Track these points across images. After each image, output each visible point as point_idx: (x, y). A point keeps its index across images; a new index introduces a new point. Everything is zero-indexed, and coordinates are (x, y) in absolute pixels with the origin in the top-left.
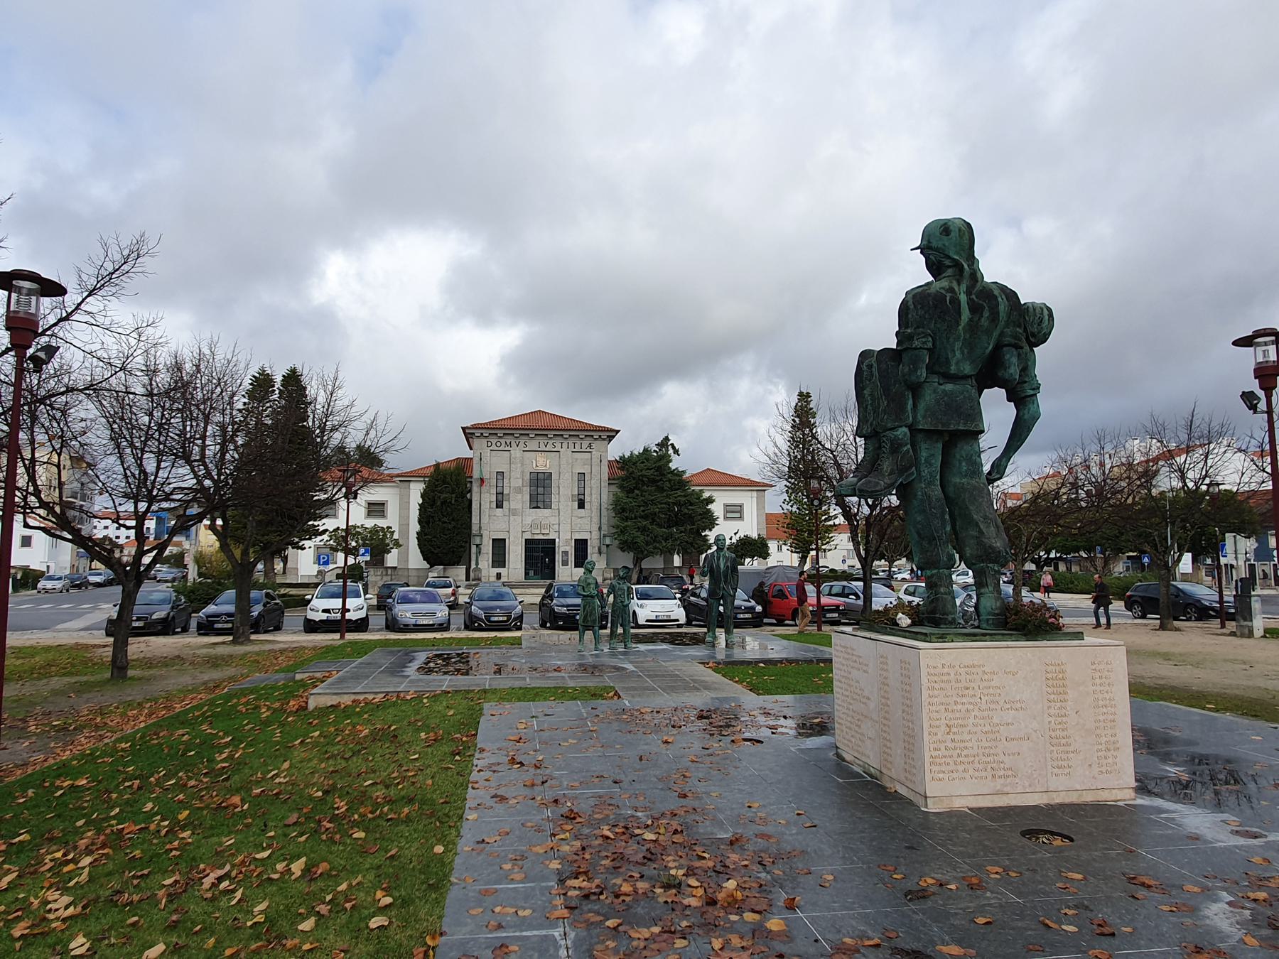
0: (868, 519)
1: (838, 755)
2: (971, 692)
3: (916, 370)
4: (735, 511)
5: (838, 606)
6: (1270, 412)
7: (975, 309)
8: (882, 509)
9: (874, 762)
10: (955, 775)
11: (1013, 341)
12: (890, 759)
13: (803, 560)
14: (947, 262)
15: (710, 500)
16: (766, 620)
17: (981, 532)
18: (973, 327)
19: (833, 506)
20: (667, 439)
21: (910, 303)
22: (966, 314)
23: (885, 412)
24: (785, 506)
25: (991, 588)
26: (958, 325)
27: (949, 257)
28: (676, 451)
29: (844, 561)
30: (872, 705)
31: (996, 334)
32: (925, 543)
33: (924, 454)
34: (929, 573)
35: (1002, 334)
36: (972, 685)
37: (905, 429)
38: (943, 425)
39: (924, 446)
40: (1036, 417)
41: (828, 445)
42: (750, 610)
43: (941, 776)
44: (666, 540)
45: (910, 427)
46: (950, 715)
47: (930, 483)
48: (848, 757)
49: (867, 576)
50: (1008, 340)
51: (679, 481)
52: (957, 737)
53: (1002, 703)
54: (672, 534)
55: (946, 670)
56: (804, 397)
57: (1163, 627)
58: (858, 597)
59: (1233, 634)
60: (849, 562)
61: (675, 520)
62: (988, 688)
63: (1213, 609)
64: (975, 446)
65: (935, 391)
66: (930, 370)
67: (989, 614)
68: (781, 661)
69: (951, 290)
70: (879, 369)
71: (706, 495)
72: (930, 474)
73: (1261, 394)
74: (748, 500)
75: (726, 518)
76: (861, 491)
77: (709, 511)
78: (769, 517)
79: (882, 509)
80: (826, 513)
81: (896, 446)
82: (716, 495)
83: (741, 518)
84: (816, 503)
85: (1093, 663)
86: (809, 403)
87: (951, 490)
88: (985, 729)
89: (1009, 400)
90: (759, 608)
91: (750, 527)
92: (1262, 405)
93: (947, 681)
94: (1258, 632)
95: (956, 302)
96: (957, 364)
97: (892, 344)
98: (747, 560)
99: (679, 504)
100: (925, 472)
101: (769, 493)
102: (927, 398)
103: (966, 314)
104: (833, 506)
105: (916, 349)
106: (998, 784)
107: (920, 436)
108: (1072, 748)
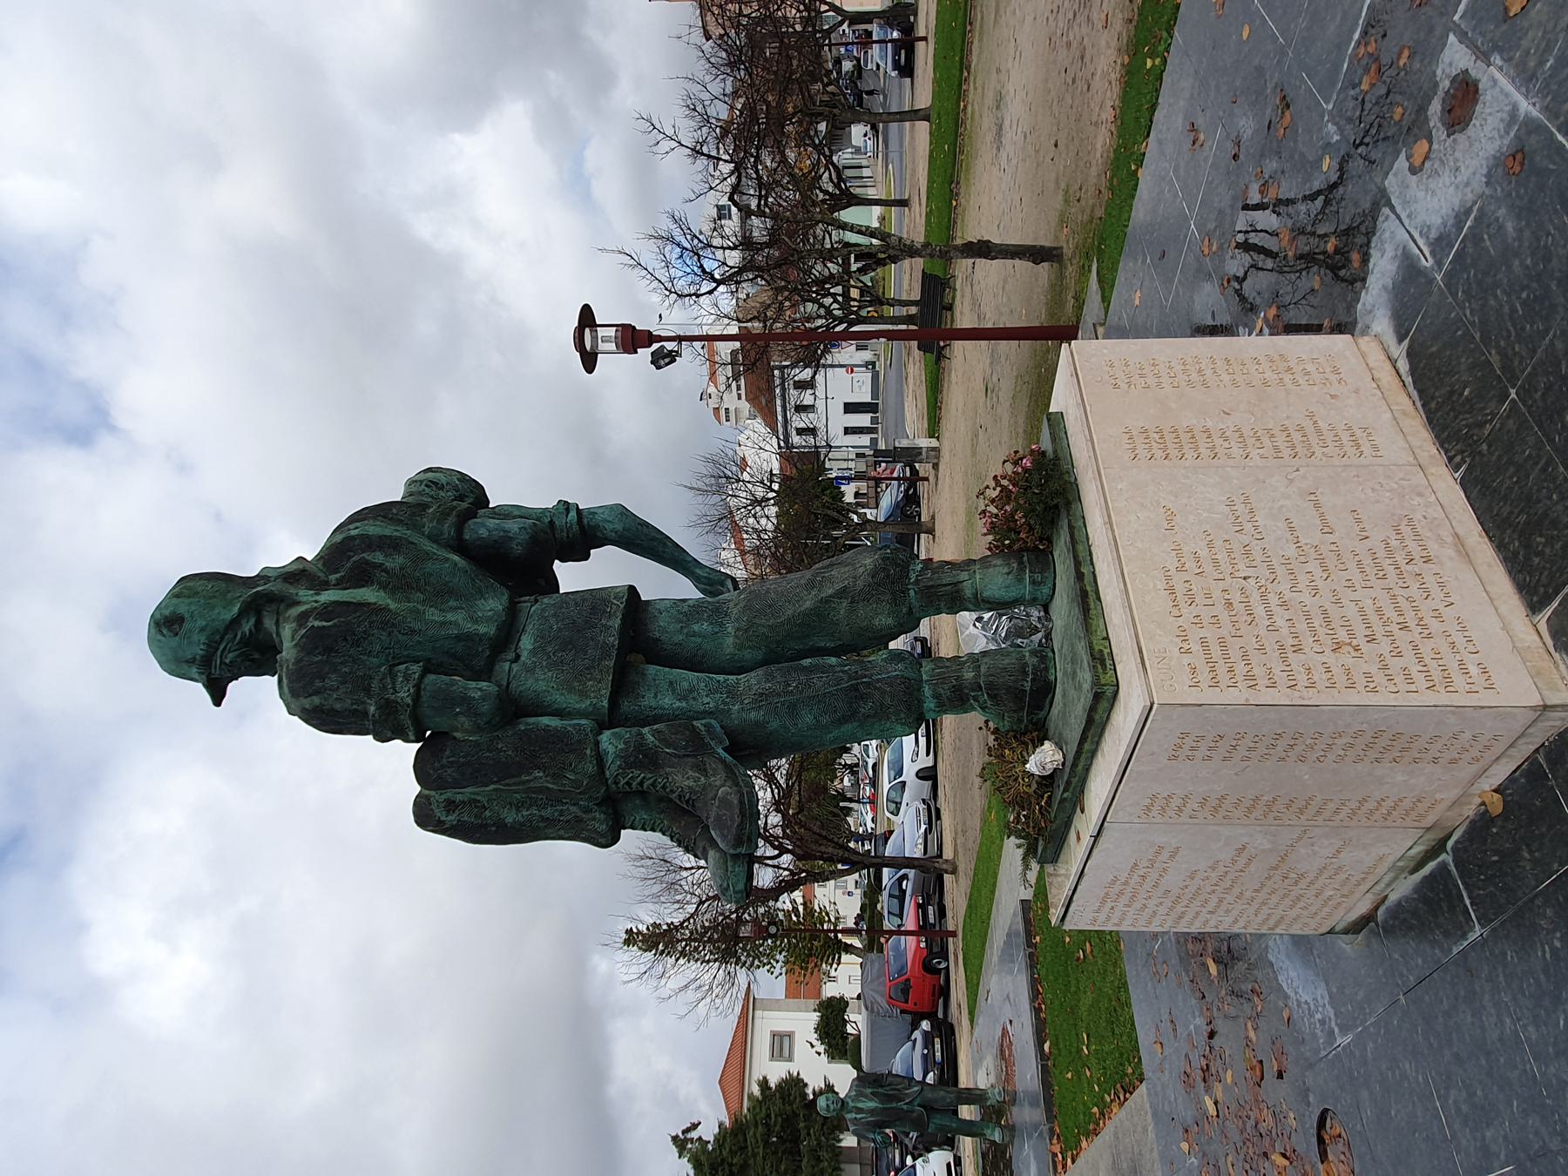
0: (798, 857)
1: (1356, 927)
2: (1236, 597)
3: (465, 700)
4: (781, 1045)
5: (919, 906)
6: (680, 339)
7: (362, 576)
8: (785, 836)
9: (1404, 843)
10: (1459, 639)
11: (452, 519)
12: (1407, 804)
13: (849, 949)
14: (247, 626)
15: (764, 1084)
16: (940, 1015)
17: (842, 593)
18: (399, 584)
19: (779, 905)
20: (675, 1139)
21: (306, 703)
22: (368, 594)
23: (557, 777)
24: (777, 972)
25: (964, 576)
26: (386, 609)
27: (235, 622)
28: (695, 1126)
29: (850, 894)
30: (1260, 842)
31: (428, 546)
32: (866, 708)
33: (668, 701)
34: (930, 704)
35: (434, 538)
36: (1217, 594)
37: (606, 736)
38: (605, 655)
39: (648, 700)
40: (622, 512)
41: (691, 909)
42: (928, 1040)
43: (1474, 670)
44: (818, 1160)
45: (602, 726)
46: (1307, 642)
47: (732, 693)
48: (1363, 908)
49: (875, 864)
50: (448, 528)
51: (733, 1134)
52: (1360, 631)
53: (1245, 539)
54: (813, 1151)
55: (1196, 647)
56: (631, 938)
57: (931, 531)
58: (905, 877)
59: (936, 466)
60: (851, 887)
61: (791, 1140)
62: (1215, 562)
63: (907, 491)
64: (661, 606)
65: (530, 670)
66: (485, 673)
67: (1020, 580)
68: (1037, 1011)
69: (302, 618)
70: (457, 784)
71: (756, 1090)
72: (710, 692)
73: (656, 346)
74: (767, 1023)
75: (790, 1059)
76: (738, 842)
77: (779, 1086)
78: (791, 993)
79: (785, 836)
80: (788, 914)
81: (642, 757)
82: (757, 1075)
83: (790, 1035)
84: (773, 930)
85: (1116, 386)
86: (639, 933)
87: (748, 655)
88: (1318, 573)
89: (586, 557)
90: (925, 1025)
91: (803, 1023)
92: (670, 346)
93: (1222, 642)
94: (934, 443)
95: (327, 611)
96: (476, 621)
97: (404, 753)
98: (850, 1030)
99: (769, 1134)
100: (707, 702)
101: (759, 993)
102: (542, 686)
103: (368, 594)
104: (779, 905)
105: (417, 697)
106: (1446, 554)
107: (626, 706)
108: (1308, 424)
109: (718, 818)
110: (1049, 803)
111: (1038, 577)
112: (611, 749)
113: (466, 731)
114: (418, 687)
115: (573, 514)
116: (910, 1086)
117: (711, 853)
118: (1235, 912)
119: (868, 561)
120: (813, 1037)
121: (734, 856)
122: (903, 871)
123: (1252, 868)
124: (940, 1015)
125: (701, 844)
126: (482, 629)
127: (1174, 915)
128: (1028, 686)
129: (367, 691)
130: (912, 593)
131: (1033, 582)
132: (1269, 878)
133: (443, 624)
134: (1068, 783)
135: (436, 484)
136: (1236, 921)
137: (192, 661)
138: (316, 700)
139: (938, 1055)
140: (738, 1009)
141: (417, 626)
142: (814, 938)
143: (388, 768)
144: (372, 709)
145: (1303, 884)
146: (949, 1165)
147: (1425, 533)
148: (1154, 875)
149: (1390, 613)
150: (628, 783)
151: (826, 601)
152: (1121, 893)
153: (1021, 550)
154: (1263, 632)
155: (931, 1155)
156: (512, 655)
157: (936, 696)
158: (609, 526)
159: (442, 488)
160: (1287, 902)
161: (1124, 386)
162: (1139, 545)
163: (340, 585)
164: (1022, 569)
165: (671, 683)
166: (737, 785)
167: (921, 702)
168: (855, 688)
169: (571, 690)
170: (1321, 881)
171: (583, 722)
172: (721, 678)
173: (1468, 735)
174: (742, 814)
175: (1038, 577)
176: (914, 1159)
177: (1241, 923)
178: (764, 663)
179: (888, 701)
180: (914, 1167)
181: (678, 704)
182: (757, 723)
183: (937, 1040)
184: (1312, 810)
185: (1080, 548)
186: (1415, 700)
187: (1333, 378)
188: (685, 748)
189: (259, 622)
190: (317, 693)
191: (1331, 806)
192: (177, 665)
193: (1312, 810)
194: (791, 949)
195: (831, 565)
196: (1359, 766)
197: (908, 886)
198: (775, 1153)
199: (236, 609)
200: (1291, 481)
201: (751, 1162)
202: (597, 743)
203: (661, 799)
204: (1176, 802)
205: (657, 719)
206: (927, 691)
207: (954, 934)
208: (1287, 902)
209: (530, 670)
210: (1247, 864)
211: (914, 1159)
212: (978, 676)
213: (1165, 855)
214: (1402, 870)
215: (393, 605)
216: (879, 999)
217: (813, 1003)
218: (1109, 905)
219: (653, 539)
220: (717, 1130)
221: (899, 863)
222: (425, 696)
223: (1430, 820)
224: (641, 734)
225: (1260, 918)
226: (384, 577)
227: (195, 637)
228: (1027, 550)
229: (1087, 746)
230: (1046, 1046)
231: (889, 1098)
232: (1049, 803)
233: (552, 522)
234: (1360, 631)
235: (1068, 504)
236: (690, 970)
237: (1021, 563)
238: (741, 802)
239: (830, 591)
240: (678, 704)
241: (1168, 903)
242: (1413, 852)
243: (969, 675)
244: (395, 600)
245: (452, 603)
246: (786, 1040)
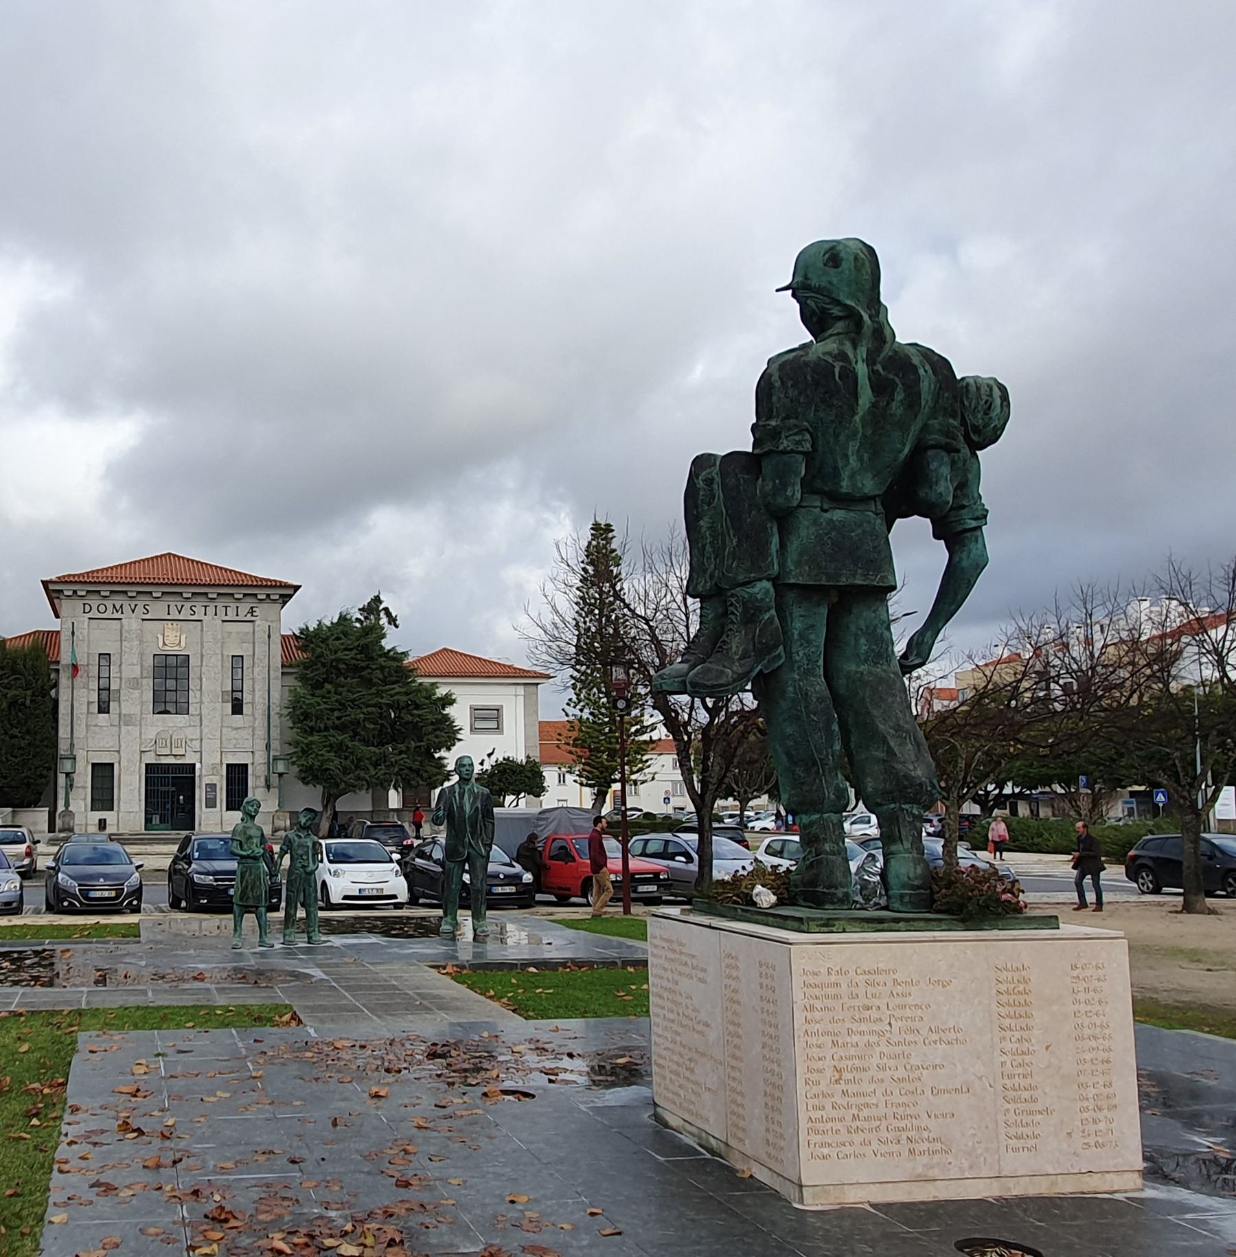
0: (705, 730)
1: (657, 1117)
2: (874, 1014)
3: (784, 486)
4: (488, 719)
5: (657, 874)
7: (881, 387)
8: (729, 715)
9: (715, 1128)
12: (742, 1124)
13: (600, 798)
14: (836, 311)
15: (448, 701)
16: (539, 897)
17: (890, 752)
18: (877, 416)
19: (649, 710)
20: (377, 600)
21: (775, 377)
22: (866, 396)
23: (733, 556)
25: (907, 845)
27: (838, 303)
28: (392, 621)
29: (667, 800)
30: (712, 1036)
31: (915, 428)
32: (799, 771)
33: (797, 625)
34: (805, 819)
35: (925, 428)
36: (876, 1002)
37: (767, 585)
39: (797, 611)
41: (640, 611)
42: (514, 879)
43: (825, 1151)
44: (376, 765)
45: (774, 581)
47: (808, 672)
48: (673, 1121)
49: (705, 825)
50: (934, 438)
51: (396, 669)
52: (852, 1088)
55: (833, 978)
56: (602, 531)
57: (1188, 908)
58: (689, 859)
60: (676, 802)
61: (391, 734)
62: (903, 1007)
64: (882, 611)
66: (808, 487)
67: (904, 886)
70: (724, 486)
71: (441, 691)
72: (807, 656)
74: (510, 700)
75: (473, 730)
76: (694, 685)
77: (446, 718)
78: (545, 729)
79: (729, 715)
81: (752, 612)
82: (458, 692)
83: (499, 729)
84: (621, 704)
85: (1074, 967)
87: (842, 682)
89: (936, 536)
90: (528, 877)
91: (513, 744)
93: (836, 997)
95: (849, 376)
101: (545, 688)
102: (803, 533)
103: (866, 396)
104: (649, 710)
105: (784, 452)
106: (919, 1165)
109: (709, 670)
110: (735, 902)
111: (907, 899)
112: (756, 590)
113: (763, 486)
114: (793, 451)
115: (974, 524)
116: (485, 845)
117: (685, 666)
118: (666, 1034)
119: (919, 772)
120: (499, 756)
121: (684, 681)
122: (695, 856)
123: (696, 1036)
124: (539, 897)
125: (692, 658)
126: (844, 483)
127: (661, 992)
128: (820, 889)
129: (788, 417)
130: (893, 806)
131: (902, 896)
132: (690, 1049)
133: (846, 456)
134: (747, 911)
135: (989, 408)
136: (659, 1036)
137: (806, 277)
138: (778, 384)
139: (499, 890)
140: (538, 669)
141: (842, 438)
142: (612, 754)
143: (734, 433)
144: (773, 423)
145: (687, 1074)
146: (395, 897)
147: (936, 1158)
148: (687, 970)
149: (865, 1112)
150: (732, 604)
151: (885, 741)
152: (674, 951)
153: (931, 889)
154: (847, 1025)
155: (402, 878)
156: (826, 506)
157: (811, 824)
158: (964, 555)
159: (985, 414)
160: (675, 1067)
161: (1075, 973)
162: (915, 957)
163: (873, 375)
164: (913, 887)
165: (813, 626)
166: (734, 681)
167: (806, 812)
168: (815, 764)
169: (801, 554)
170: (690, 1085)
171: (776, 566)
172: (821, 662)
173: (782, 1143)
174: (713, 686)
175: (907, 899)
176: (398, 862)
177: (658, 1040)
178: (835, 696)
179: (805, 788)
180: (391, 861)
181: (796, 633)
182: (785, 692)
183: (512, 889)
184: (734, 1063)
185: (922, 924)
186: (801, 1107)
187: (1091, 1140)
188: (760, 643)
189: (839, 318)
190: (783, 383)
191: (737, 1074)
192: (803, 264)
193: (734, 1063)
194: (596, 726)
195: (918, 744)
196: (762, 1083)
197: (679, 863)
198: (381, 716)
199: (849, 302)
200: (980, 1078)
201: (373, 690)
202: (760, 580)
203: (723, 626)
204: (734, 973)
205: (782, 619)
206: (817, 816)
207: (627, 911)
208: (675, 1067)
209: (815, 522)
210: (698, 1032)
211: (398, 862)
212: (827, 853)
213: (701, 975)
214: (700, 1138)
215: (857, 418)
216: (552, 826)
217: (536, 755)
218: (665, 945)
219: (956, 593)
220: (399, 650)
221: (705, 851)
222: (786, 457)
223: (732, 1142)
224: (769, 609)
225: (664, 1053)
226: (883, 404)
227: (824, 279)
228: (932, 893)
229: (771, 919)
230: (532, 969)
231: (474, 825)
232: (735, 902)
233: (964, 507)
234: (852, 1088)
235: (963, 921)
236: (567, 606)
237: (918, 887)
238: (722, 685)
239: (892, 744)
240: (796, 633)
241: (670, 985)
242: (712, 1139)
243: (827, 847)
244: (863, 418)
245: (866, 456)
246: (493, 725)
